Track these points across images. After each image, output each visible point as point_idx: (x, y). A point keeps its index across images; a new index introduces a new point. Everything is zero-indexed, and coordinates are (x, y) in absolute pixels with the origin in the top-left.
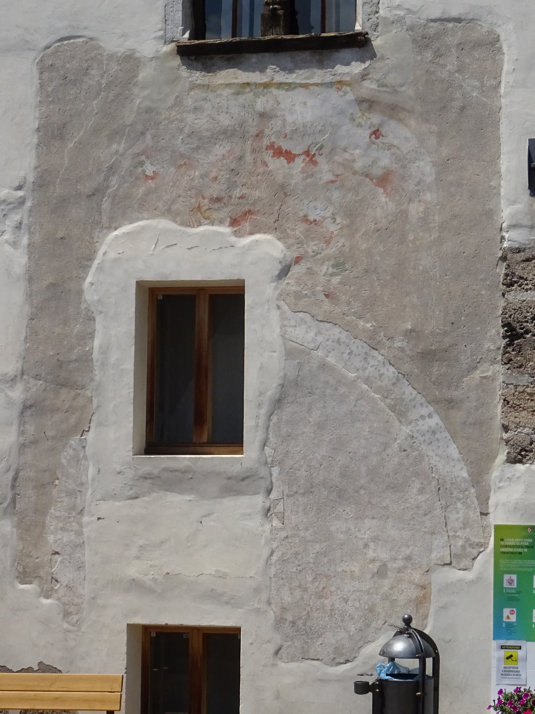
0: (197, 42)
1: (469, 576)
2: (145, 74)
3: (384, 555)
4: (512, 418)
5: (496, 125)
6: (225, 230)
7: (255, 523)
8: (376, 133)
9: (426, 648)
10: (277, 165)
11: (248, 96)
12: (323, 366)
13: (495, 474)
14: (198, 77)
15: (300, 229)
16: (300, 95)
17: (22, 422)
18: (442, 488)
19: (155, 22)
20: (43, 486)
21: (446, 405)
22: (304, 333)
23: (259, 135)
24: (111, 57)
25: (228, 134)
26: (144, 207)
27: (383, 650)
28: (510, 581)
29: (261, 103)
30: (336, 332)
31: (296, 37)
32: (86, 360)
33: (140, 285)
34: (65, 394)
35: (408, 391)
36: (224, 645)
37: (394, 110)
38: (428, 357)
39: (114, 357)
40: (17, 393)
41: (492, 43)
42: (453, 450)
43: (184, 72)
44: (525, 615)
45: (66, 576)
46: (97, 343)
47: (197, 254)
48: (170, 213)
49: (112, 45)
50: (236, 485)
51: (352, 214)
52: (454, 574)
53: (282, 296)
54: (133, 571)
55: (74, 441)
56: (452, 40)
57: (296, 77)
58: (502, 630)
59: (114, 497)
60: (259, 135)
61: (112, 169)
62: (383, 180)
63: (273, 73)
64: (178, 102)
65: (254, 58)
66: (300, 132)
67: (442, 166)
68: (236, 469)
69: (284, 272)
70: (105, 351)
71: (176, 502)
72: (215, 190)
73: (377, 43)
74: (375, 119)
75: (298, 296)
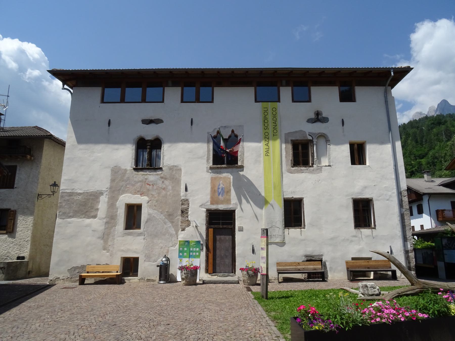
0: (11, 282)
1: (175, 248)
2: (128, 172)
3: (162, 245)
4: (182, 224)
5: (181, 181)
6: (139, 196)
7: (142, 241)
8: (163, 182)
9: (168, 260)
10: (148, 186)
11: (144, 176)
12: (154, 216)
13: (179, 233)
14: (136, 173)
15: (151, 196)
16: (151, 176)
17: (105, 225)
18: (171, 235)
19: (130, 165)
20: (108, 234)
21: (172, 222)
22: (151, 211)
23: (145, 182)
24: (123, 169)
25: (140, 181)
26: (127, 192)
27: (161, 260)
28: (181, 249)
29: (146, 177)
30: (156, 211)
31: (389, 80)
32: (116, 215)
33: (126, 204)
34: (113, 221)
35: (166, 220)
36: (136, 260)
37: (166, 179)
38: (170, 215)
39: (121, 215)
40: (105, 220)
41: (181, 170)
42: (173, 229)
43: (134, 172)
44: (183, 254)
45: (111, 249)
46: (118, 213)
47: (134, 199)
48: (131, 193)
49: (123, 167)
50: (140, 235)
51: (159, 194)
52: (173, 248)
53: (148, 206)
54: (122, 248)
55: (114, 228)
56: (175, 169)
57: (151, 173)
58: (180, 256)
59: (119, 237)
60: (145, 182)
61: (122, 186)
62: (164, 189)
63: (148, 173)
64: (133, 176)
65: (145, 170)
66: (152, 181)
67: (173, 187)
68: (139, 232)
69: (148, 202)
70: (119, 214)
71: (130, 237)
72: (138, 190)
73: (163, 169)
74: (163, 180)
75: (150, 206)
